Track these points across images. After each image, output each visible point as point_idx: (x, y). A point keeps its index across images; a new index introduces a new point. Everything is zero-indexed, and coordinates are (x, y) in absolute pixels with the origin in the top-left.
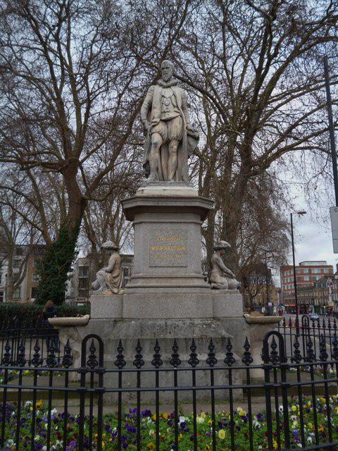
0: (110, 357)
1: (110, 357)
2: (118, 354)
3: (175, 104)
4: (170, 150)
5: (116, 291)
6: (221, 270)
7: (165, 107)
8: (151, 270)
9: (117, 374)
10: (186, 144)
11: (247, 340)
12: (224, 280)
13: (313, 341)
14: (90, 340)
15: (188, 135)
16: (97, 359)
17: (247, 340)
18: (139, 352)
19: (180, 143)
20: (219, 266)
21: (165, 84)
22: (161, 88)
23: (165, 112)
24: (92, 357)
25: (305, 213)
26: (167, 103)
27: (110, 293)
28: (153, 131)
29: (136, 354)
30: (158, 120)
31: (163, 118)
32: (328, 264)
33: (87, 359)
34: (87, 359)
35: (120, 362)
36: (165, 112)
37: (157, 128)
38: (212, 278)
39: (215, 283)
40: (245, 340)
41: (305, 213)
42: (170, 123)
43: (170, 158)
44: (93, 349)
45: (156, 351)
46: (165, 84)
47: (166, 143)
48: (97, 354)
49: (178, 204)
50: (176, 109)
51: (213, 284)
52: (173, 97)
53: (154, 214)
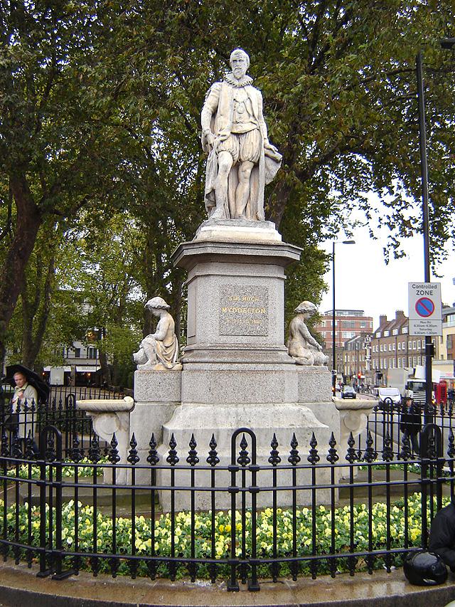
0: (264, 452)
1: (264, 452)
2: (131, 449)
3: (251, 113)
4: (241, 175)
5: (170, 365)
6: (306, 339)
7: (237, 116)
8: (224, 339)
9: (271, 472)
10: (264, 168)
11: (213, 437)
12: (309, 353)
13: (373, 439)
14: (241, 435)
15: (266, 155)
16: (250, 455)
17: (213, 437)
18: (213, 448)
19: (256, 166)
20: (303, 336)
21: (237, 83)
22: (231, 87)
23: (237, 123)
24: (244, 454)
25: (344, 242)
26: (240, 109)
27: (162, 368)
28: (221, 147)
29: (335, 448)
30: (228, 133)
31: (235, 131)
32: (365, 315)
33: (238, 455)
34: (238, 455)
35: (275, 458)
36: (237, 123)
37: (227, 145)
38: (293, 351)
39: (297, 356)
40: (311, 437)
41: (344, 242)
42: (243, 138)
43: (240, 186)
44: (244, 444)
45: (211, 447)
46: (237, 83)
47: (237, 165)
48: (249, 450)
49: (260, 253)
50: (252, 119)
51: (294, 360)
52: (248, 102)
53: (225, 265)
